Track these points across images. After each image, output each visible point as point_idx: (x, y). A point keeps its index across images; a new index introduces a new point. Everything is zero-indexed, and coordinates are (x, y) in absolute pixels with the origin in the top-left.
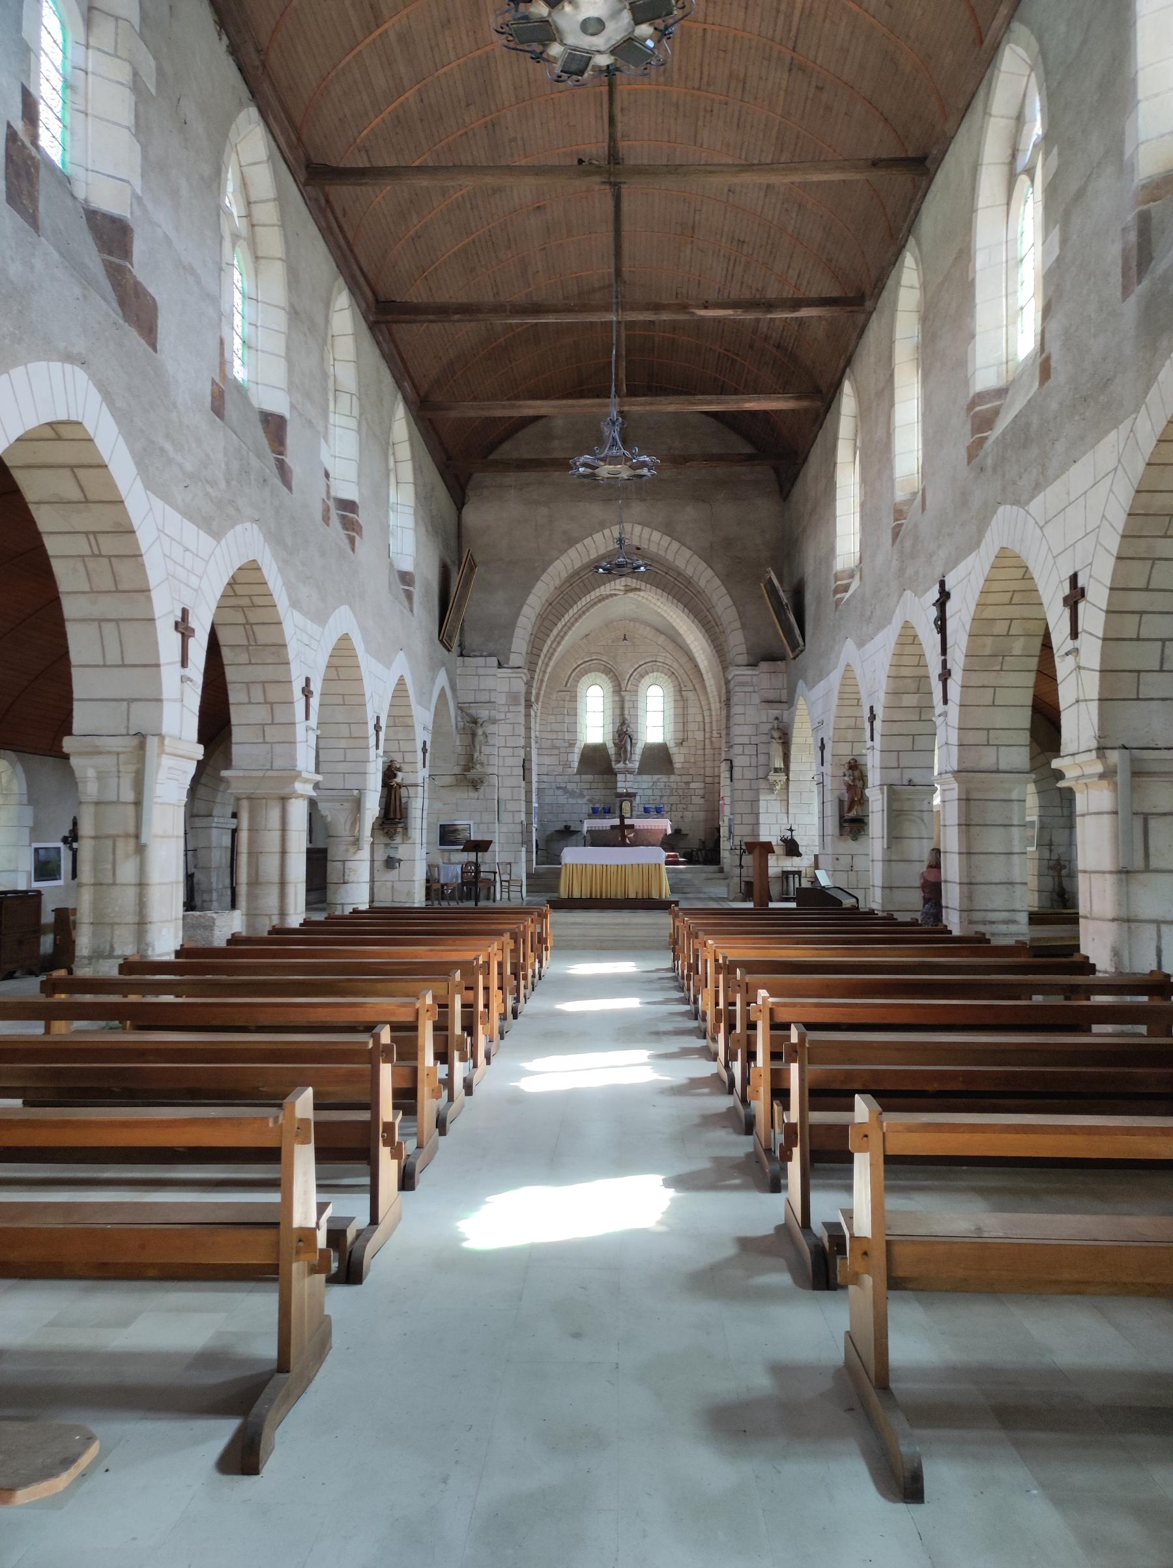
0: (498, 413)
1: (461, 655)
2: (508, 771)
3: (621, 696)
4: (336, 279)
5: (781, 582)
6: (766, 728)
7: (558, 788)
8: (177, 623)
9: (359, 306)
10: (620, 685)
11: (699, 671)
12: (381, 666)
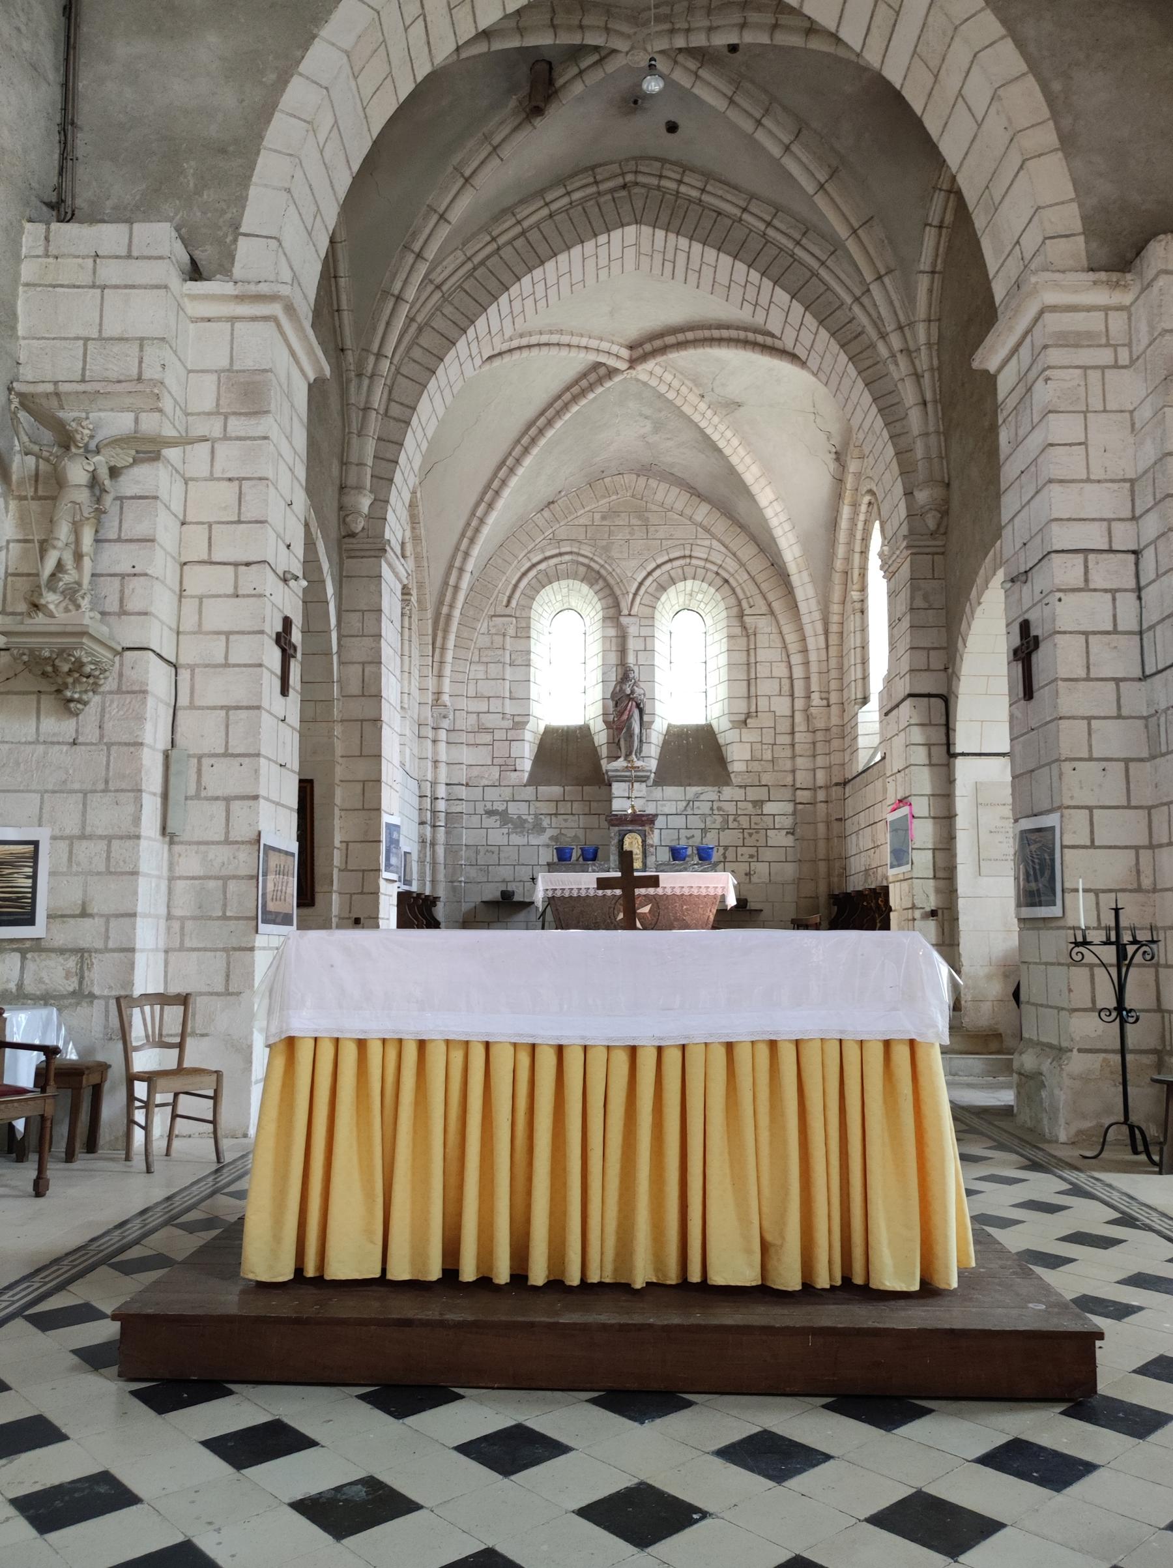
7: (490, 813)
10: (617, 605)
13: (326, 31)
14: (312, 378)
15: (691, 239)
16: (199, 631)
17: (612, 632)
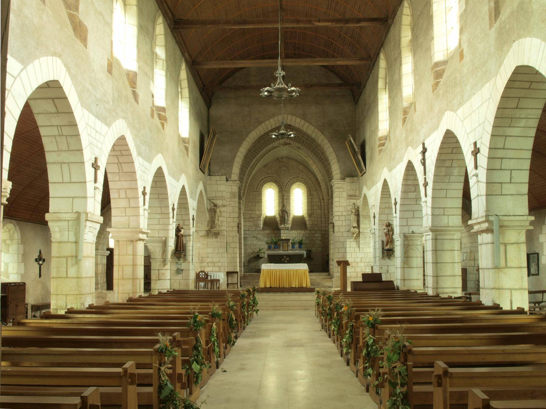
0: (227, 66)
1: (209, 175)
3: (282, 193)
4: (158, 11)
5: (355, 142)
6: (349, 208)
8: (93, 164)
9: (167, 21)
11: (319, 182)
12: (174, 181)
13: (242, 145)
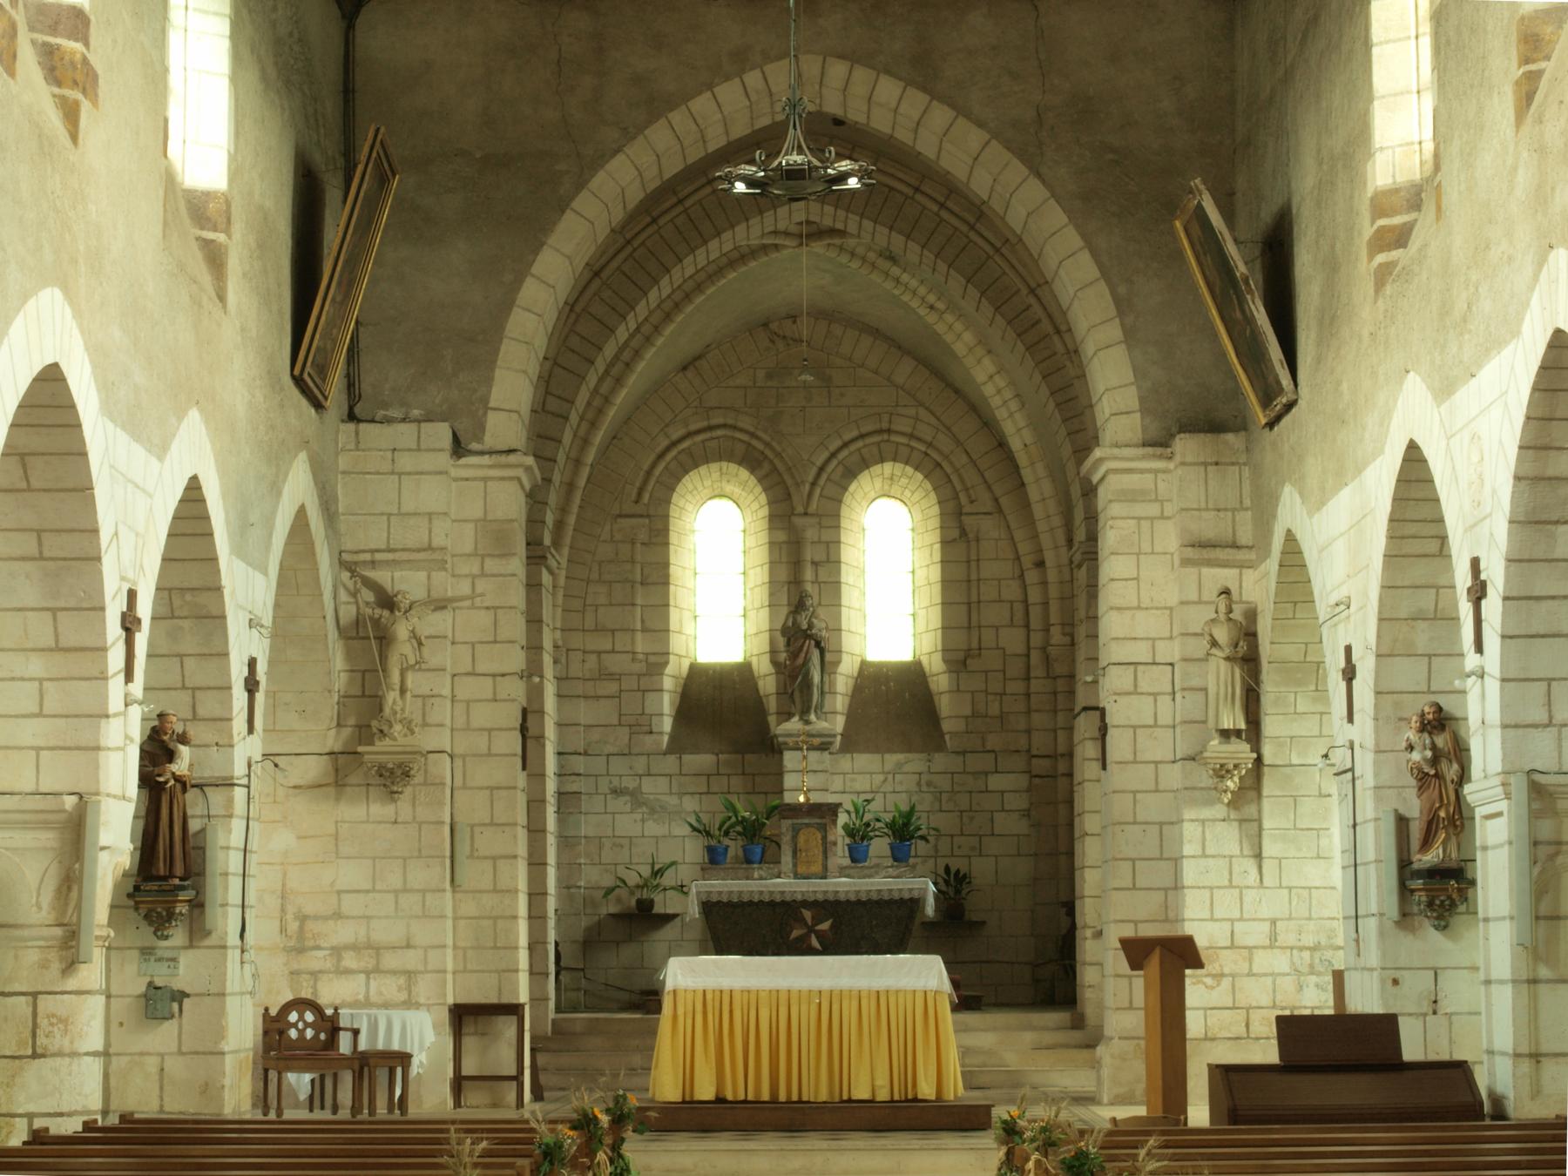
1: (352, 417)
2: (481, 743)
3: (791, 529)
5: (1229, 215)
6: (1198, 618)
11: (1010, 458)
12: (139, 451)
14: (528, 486)
15: (862, 216)
16: (468, 728)
17: (781, 536)
